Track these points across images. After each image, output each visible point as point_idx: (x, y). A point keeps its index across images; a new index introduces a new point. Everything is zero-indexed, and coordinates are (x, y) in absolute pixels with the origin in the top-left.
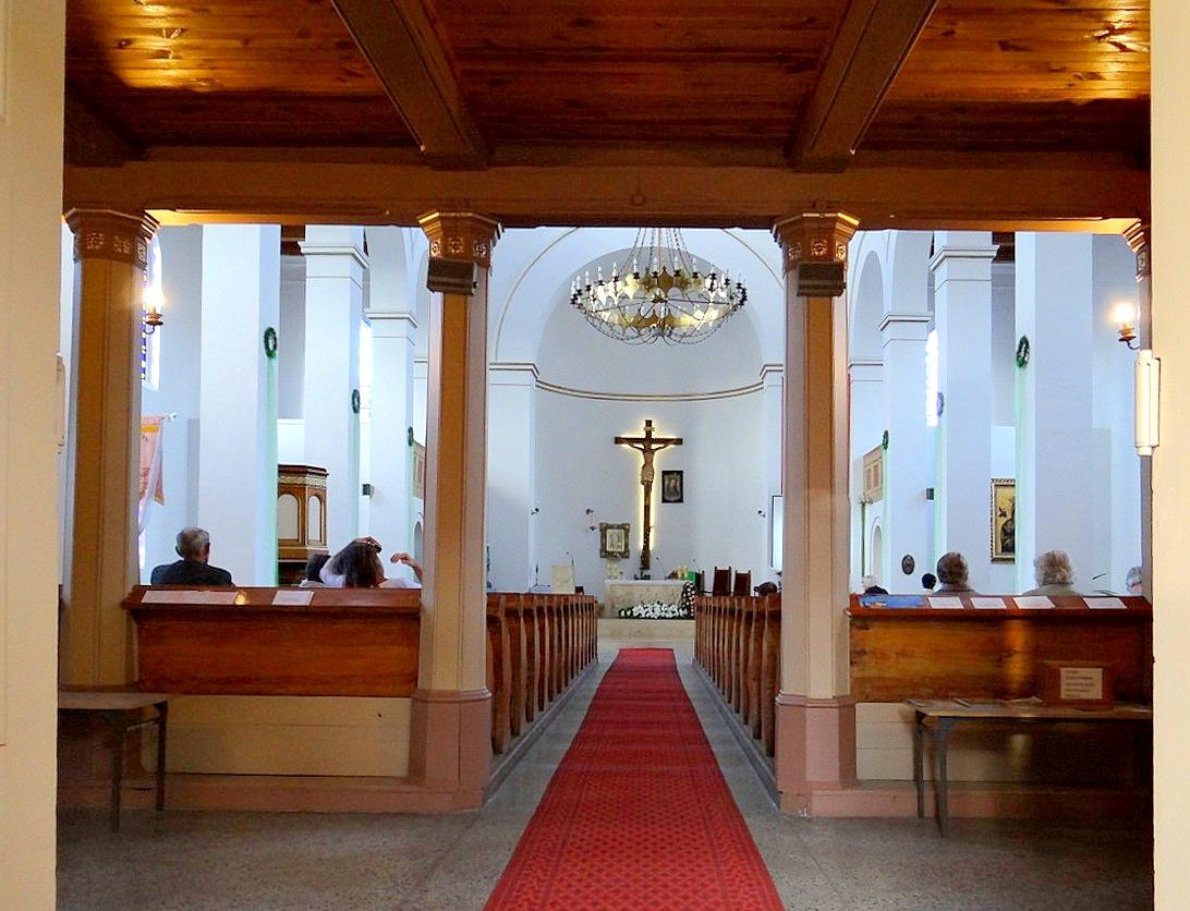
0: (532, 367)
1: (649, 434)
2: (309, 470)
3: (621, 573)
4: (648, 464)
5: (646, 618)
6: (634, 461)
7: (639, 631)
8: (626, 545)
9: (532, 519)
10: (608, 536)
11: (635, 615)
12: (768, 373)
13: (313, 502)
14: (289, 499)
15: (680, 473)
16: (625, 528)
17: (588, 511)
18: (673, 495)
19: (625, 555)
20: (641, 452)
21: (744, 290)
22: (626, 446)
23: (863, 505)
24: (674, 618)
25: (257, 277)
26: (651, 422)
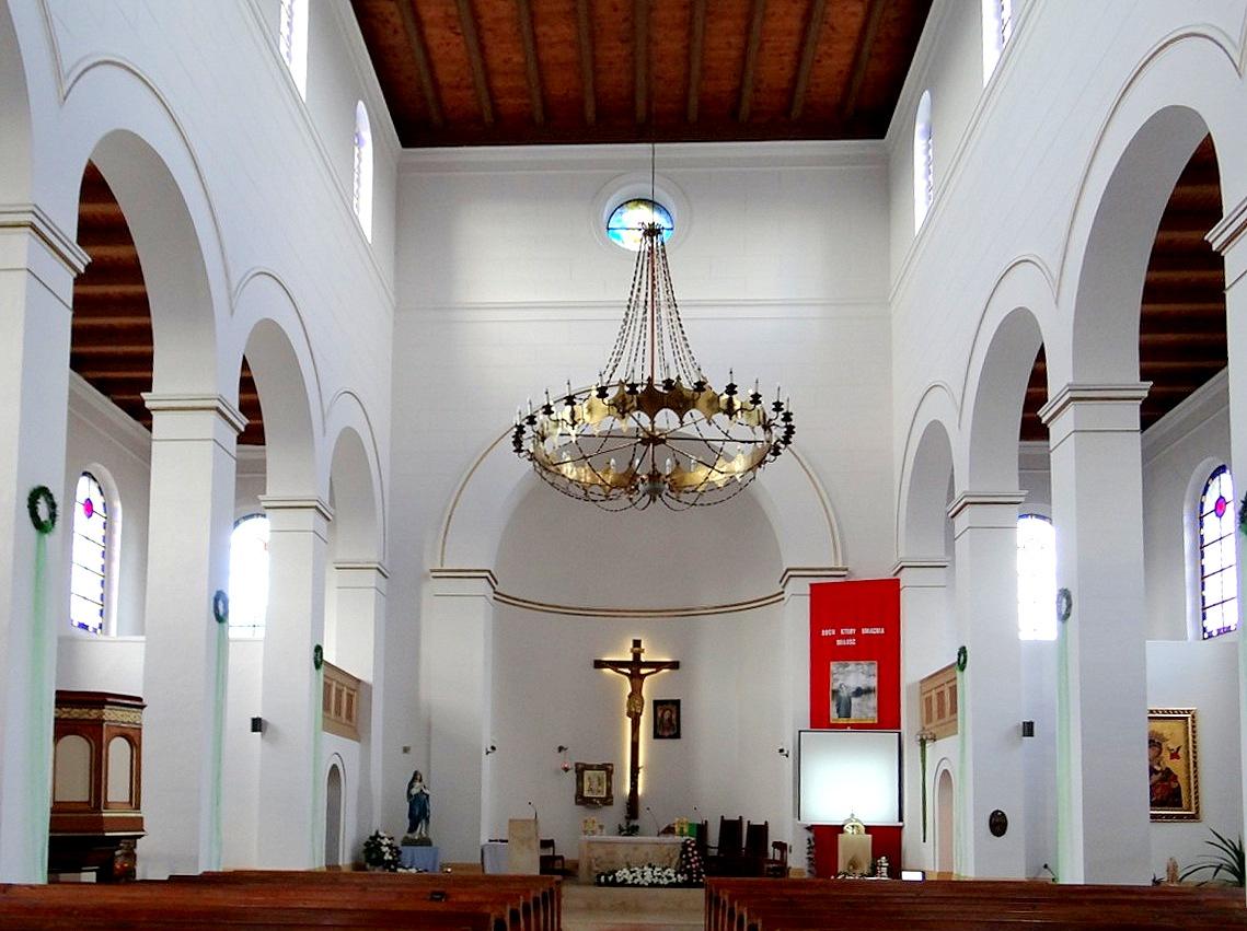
0: (487, 574)
1: (637, 656)
2: (110, 700)
3: (601, 827)
4: (636, 691)
5: (633, 885)
6: (619, 688)
7: (623, 903)
8: (609, 790)
9: (487, 761)
10: (585, 779)
11: (619, 880)
12: (792, 579)
13: (118, 750)
14: (77, 746)
15: (677, 703)
16: (608, 769)
17: (561, 749)
18: (668, 729)
19: (607, 801)
20: (627, 678)
21: (787, 417)
22: (608, 671)
23: (923, 743)
24: (671, 885)
25: (17, 408)
26: (640, 641)
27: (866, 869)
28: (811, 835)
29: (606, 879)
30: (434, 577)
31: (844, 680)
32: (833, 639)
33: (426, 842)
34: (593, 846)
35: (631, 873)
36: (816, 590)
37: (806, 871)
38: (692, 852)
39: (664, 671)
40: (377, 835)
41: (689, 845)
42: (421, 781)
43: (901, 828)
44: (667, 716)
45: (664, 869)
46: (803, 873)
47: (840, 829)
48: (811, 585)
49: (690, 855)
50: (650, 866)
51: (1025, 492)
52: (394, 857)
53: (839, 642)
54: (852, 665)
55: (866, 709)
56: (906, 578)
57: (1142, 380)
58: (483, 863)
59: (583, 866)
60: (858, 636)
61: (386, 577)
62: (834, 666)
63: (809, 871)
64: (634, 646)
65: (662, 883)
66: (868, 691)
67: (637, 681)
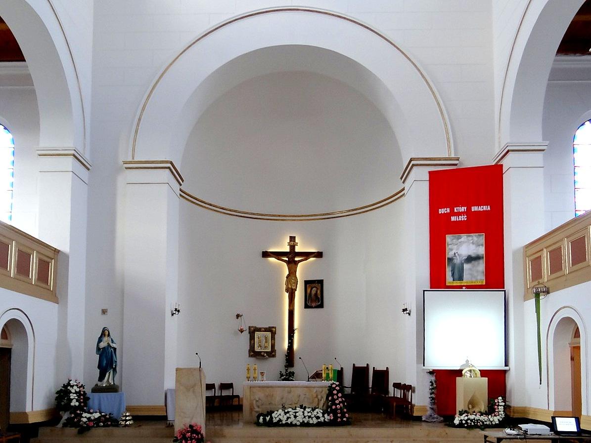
0: (169, 165)
1: (292, 247)
4: (292, 273)
5: (287, 425)
8: (273, 346)
11: (275, 420)
15: (321, 282)
16: (272, 330)
19: (272, 354)
20: (285, 264)
22: (272, 260)
24: (319, 425)
27: (483, 407)
28: (433, 378)
29: (264, 419)
30: (126, 168)
31: (458, 249)
32: (448, 216)
33: (112, 389)
34: (254, 390)
35: (286, 413)
36: (434, 177)
37: (428, 408)
38: (337, 394)
39: (312, 259)
40: (69, 384)
41: (334, 389)
42: (109, 335)
43: (505, 372)
44: (314, 292)
45: (313, 410)
46: (427, 411)
47: (459, 373)
48: (430, 173)
49: (335, 397)
50: (301, 407)
51: (547, 143)
52: (80, 403)
53: (453, 219)
54: (464, 237)
55: (476, 273)
56: (506, 163)
57: (543, 140)
58: (166, 405)
59: (246, 408)
60: (468, 213)
61: (88, 169)
62: (449, 238)
63: (432, 409)
64: (291, 241)
65: (311, 422)
66: (478, 258)
67: (292, 265)
